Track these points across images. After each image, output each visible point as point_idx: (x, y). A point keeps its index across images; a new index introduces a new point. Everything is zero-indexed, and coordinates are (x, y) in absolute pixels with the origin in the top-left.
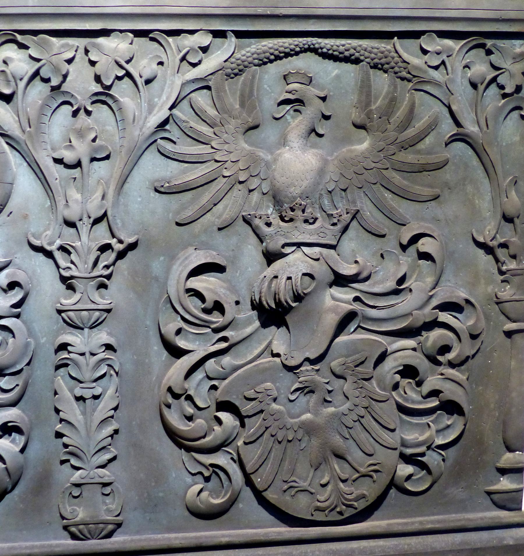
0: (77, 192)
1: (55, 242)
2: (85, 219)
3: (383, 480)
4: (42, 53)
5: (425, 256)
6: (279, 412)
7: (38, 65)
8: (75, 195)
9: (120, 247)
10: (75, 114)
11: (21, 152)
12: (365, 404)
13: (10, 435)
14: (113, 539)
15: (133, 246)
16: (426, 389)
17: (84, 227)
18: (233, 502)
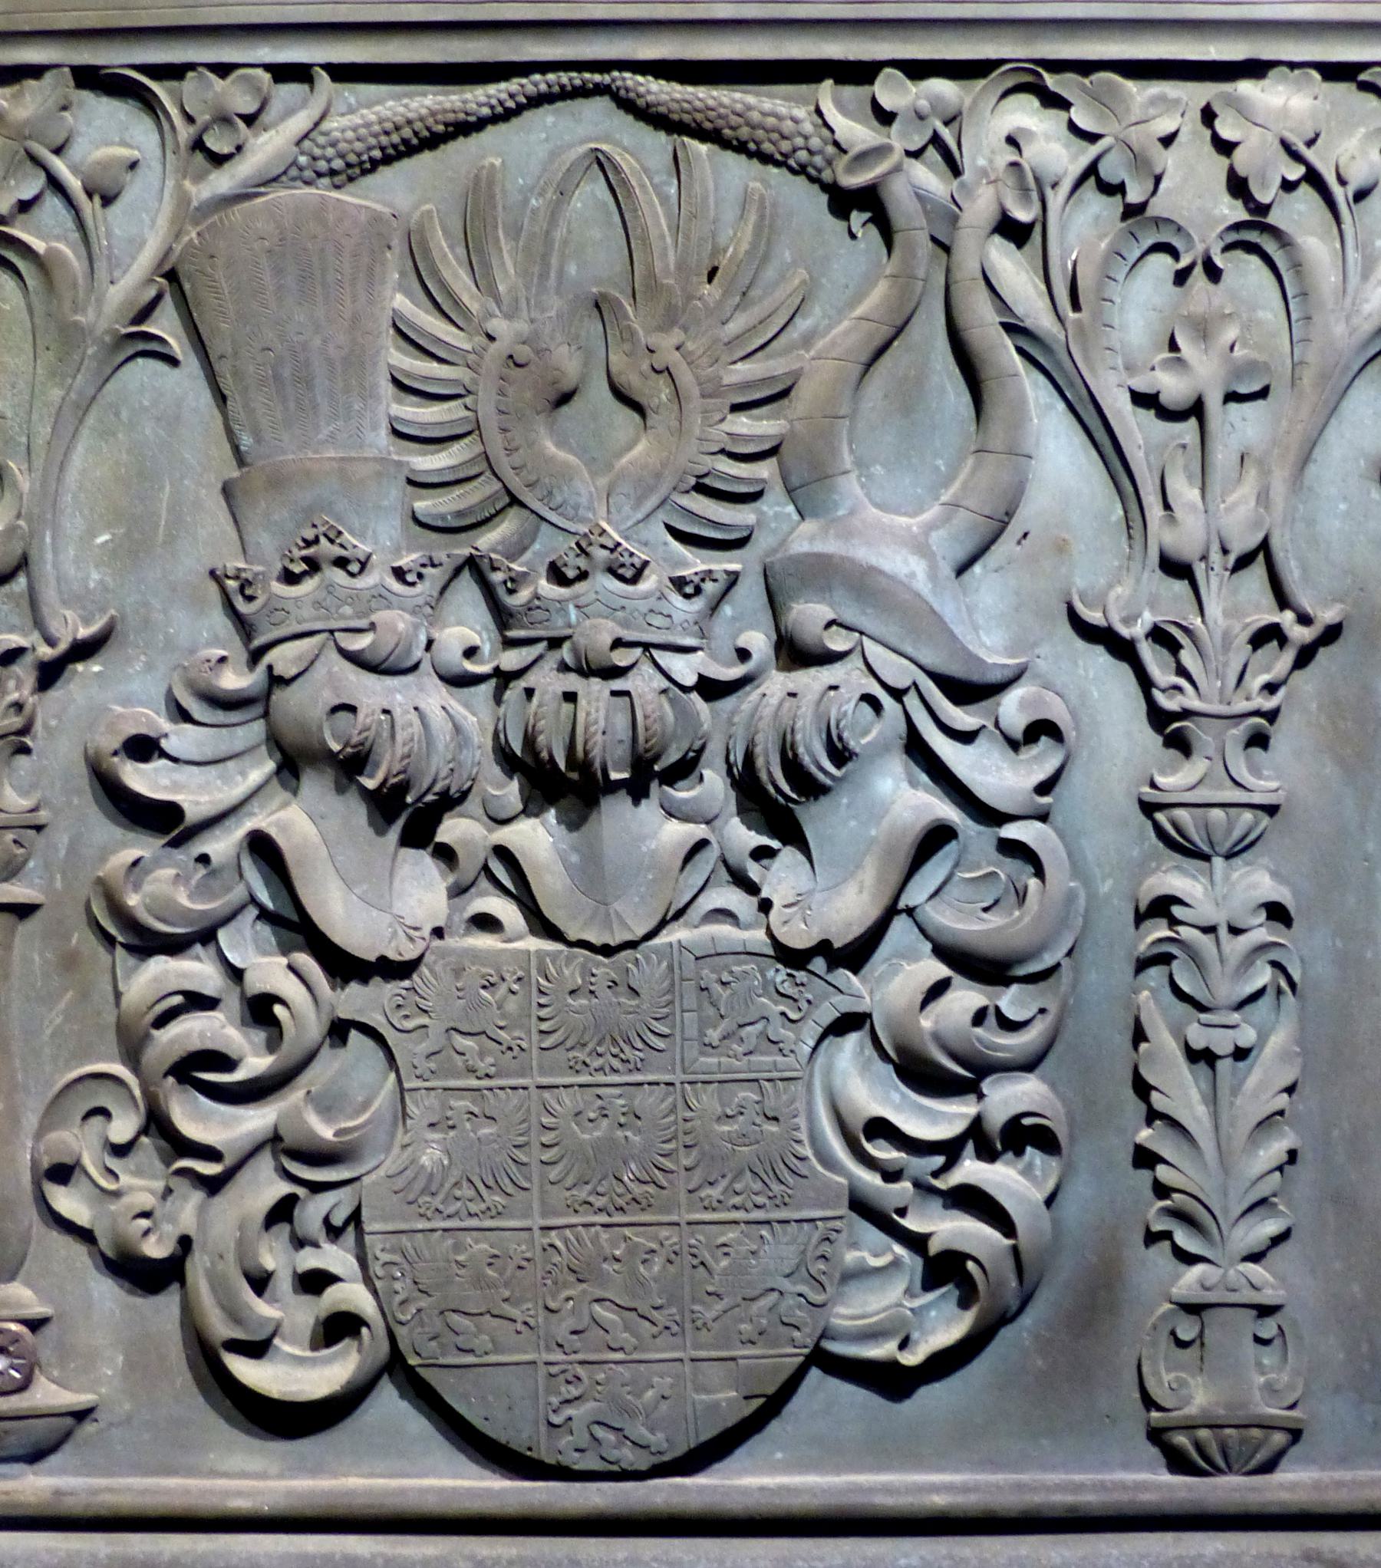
0: (1191, 484)
1: (1139, 615)
2: (1215, 556)
4: (1101, 118)
7: (1094, 150)
9: (1301, 634)
10: (1181, 277)
11: (1055, 374)
13: (1019, 1153)
14: (1284, 1476)
15: (1332, 634)
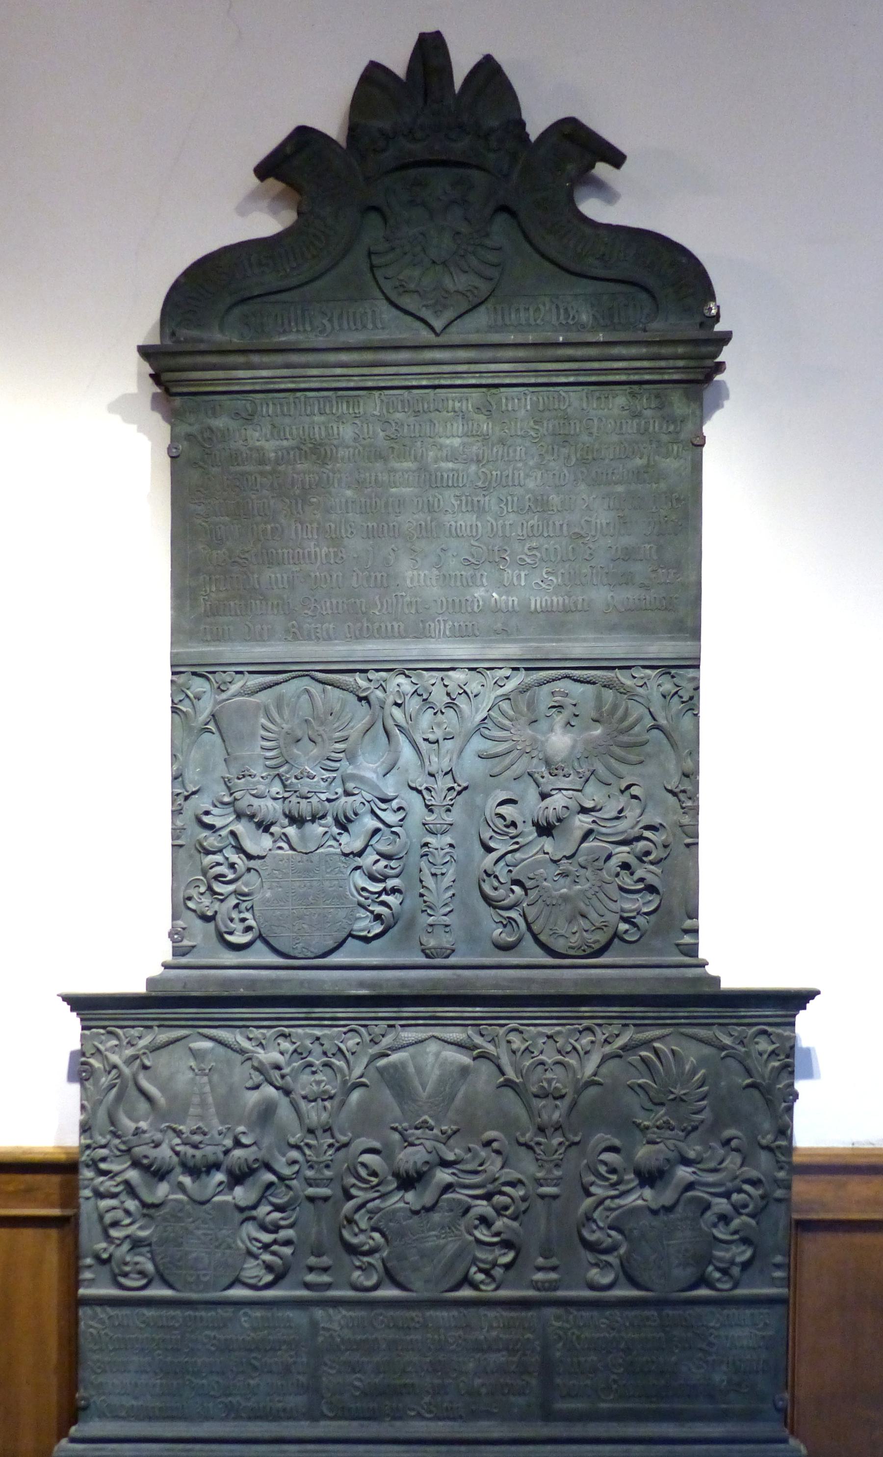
3: (610, 932)
5: (635, 797)
6: (548, 887)
7: (417, 687)
8: (434, 759)
9: (458, 788)
10: (435, 714)
12: (599, 884)
15: (466, 788)
16: (636, 876)
17: (439, 777)
18: (519, 940)
